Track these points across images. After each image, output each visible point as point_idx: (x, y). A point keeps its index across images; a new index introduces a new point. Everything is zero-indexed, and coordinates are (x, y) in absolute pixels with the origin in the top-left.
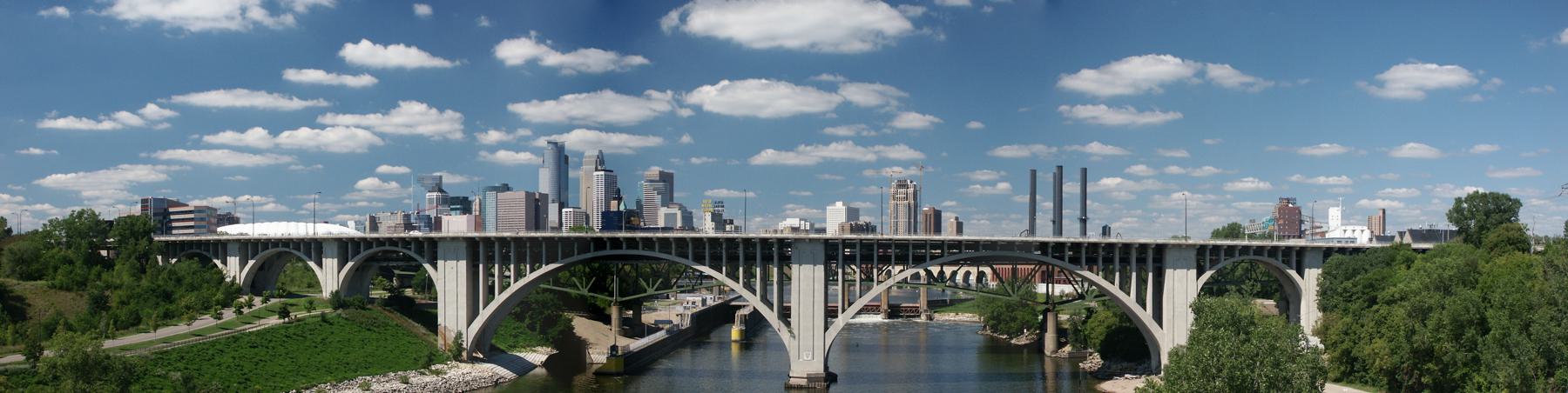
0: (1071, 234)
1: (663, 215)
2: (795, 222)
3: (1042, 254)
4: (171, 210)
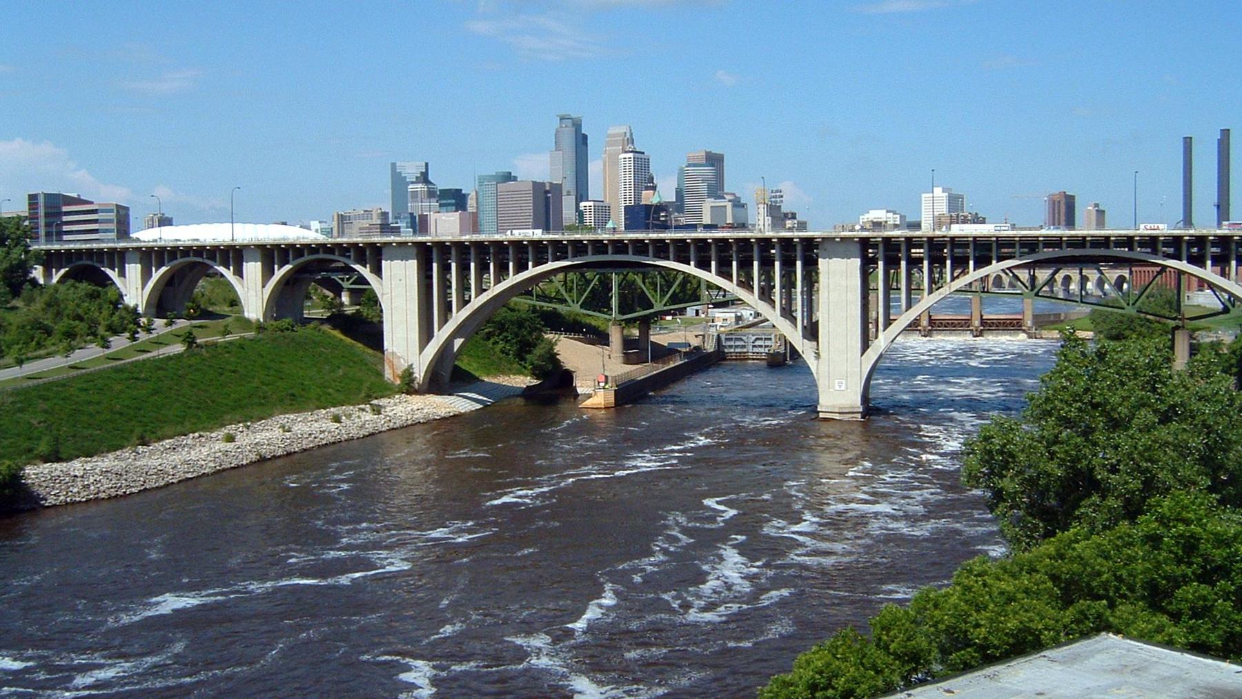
1: (709, 209)
2: (879, 215)
3: (1129, 250)
4: (65, 209)
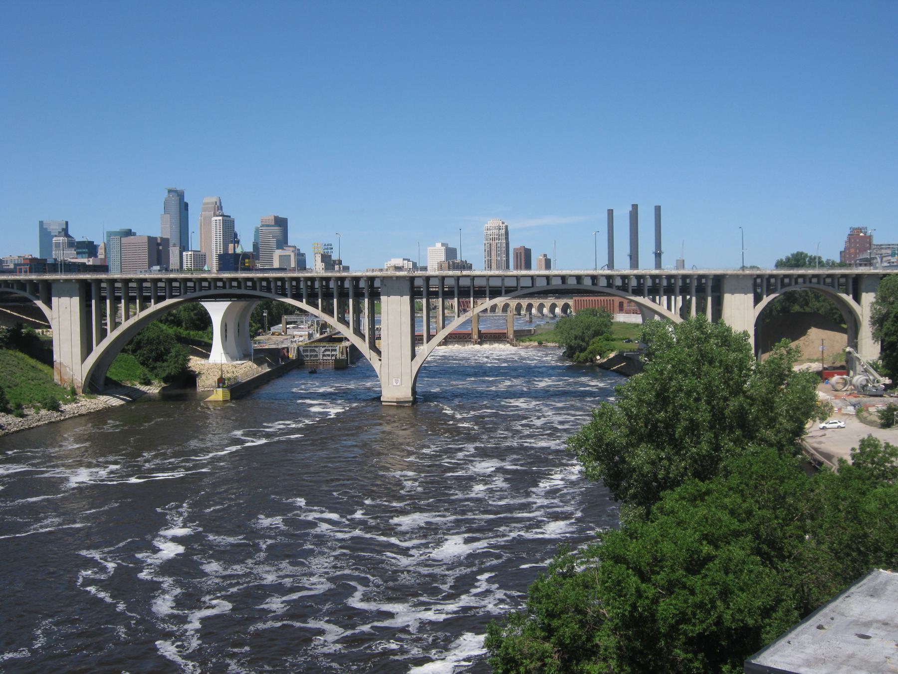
0: (647, 267)
2: (399, 262)
